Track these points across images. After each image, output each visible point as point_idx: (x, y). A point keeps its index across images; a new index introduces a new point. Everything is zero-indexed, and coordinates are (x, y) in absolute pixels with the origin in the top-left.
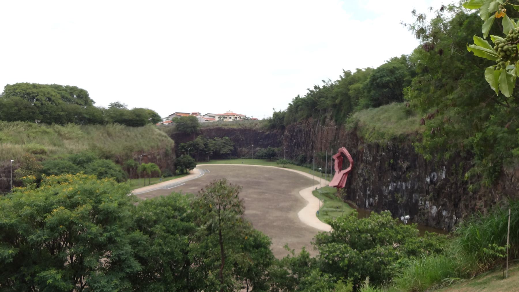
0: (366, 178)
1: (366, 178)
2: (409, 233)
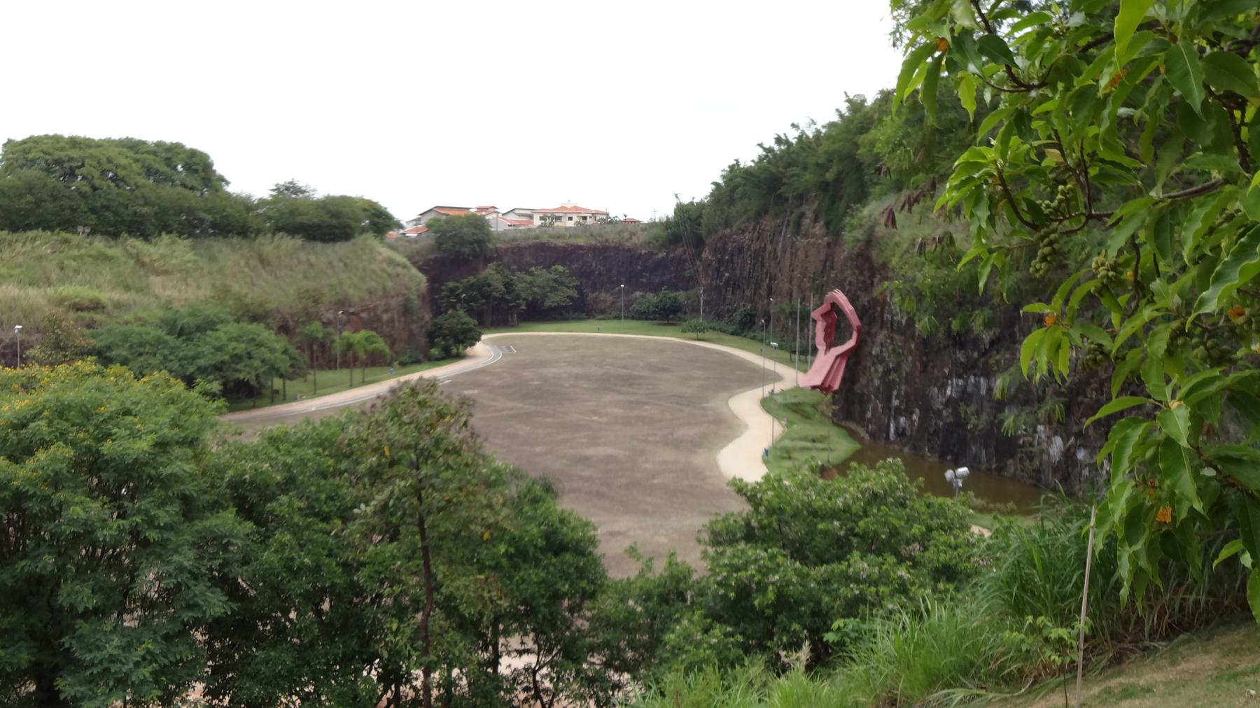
0: (891, 365)
1: (891, 365)
2: (946, 518)
